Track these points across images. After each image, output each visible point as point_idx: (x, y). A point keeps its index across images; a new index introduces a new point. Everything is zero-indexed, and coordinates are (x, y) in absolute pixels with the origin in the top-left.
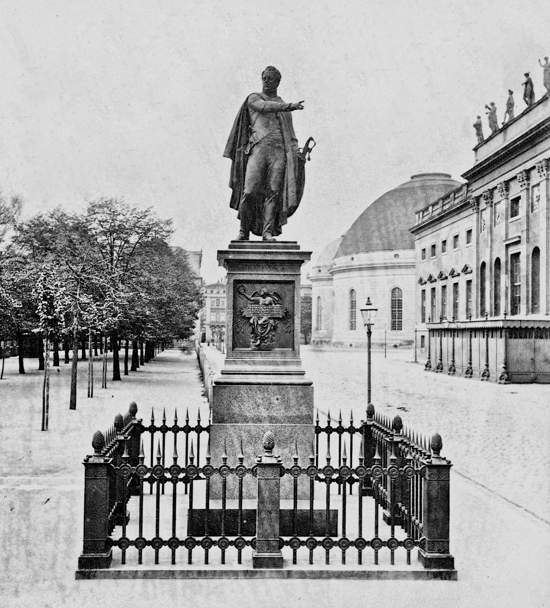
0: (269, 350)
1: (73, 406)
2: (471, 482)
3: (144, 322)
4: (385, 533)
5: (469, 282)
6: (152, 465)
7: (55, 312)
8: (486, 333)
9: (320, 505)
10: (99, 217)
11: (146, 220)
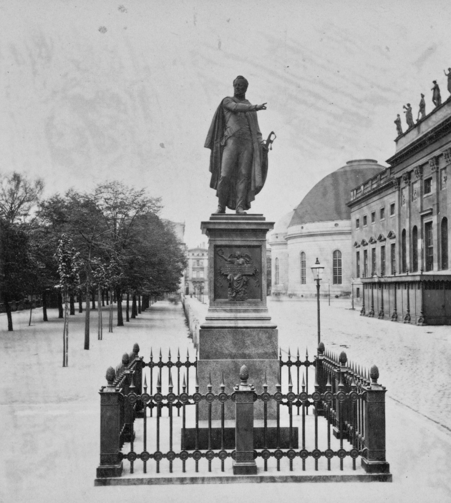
0: (242, 300)
1: (87, 347)
2: (400, 404)
3: (142, 279)
4: (336, 445)
5: (393, 245)
6: (298, 393)
7: (72, 272)
8: (407, 286)
9: (284, 423)
10: (106, 195)
11: (142, 198)
